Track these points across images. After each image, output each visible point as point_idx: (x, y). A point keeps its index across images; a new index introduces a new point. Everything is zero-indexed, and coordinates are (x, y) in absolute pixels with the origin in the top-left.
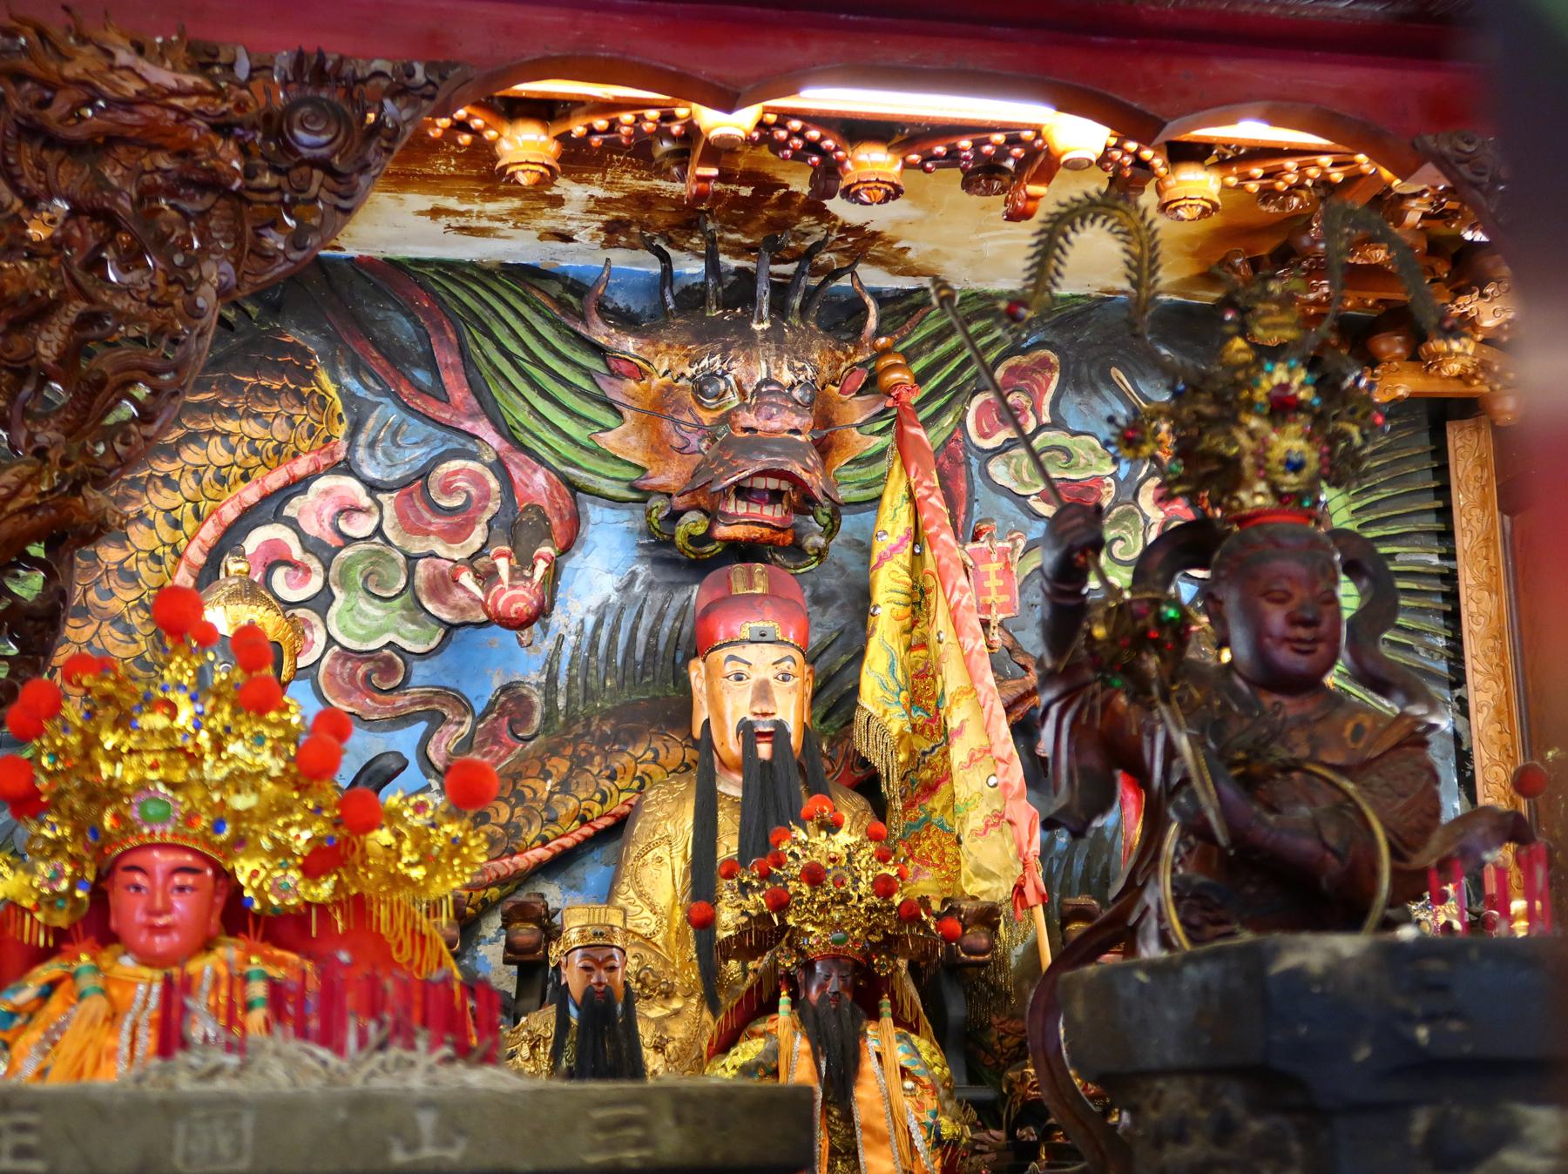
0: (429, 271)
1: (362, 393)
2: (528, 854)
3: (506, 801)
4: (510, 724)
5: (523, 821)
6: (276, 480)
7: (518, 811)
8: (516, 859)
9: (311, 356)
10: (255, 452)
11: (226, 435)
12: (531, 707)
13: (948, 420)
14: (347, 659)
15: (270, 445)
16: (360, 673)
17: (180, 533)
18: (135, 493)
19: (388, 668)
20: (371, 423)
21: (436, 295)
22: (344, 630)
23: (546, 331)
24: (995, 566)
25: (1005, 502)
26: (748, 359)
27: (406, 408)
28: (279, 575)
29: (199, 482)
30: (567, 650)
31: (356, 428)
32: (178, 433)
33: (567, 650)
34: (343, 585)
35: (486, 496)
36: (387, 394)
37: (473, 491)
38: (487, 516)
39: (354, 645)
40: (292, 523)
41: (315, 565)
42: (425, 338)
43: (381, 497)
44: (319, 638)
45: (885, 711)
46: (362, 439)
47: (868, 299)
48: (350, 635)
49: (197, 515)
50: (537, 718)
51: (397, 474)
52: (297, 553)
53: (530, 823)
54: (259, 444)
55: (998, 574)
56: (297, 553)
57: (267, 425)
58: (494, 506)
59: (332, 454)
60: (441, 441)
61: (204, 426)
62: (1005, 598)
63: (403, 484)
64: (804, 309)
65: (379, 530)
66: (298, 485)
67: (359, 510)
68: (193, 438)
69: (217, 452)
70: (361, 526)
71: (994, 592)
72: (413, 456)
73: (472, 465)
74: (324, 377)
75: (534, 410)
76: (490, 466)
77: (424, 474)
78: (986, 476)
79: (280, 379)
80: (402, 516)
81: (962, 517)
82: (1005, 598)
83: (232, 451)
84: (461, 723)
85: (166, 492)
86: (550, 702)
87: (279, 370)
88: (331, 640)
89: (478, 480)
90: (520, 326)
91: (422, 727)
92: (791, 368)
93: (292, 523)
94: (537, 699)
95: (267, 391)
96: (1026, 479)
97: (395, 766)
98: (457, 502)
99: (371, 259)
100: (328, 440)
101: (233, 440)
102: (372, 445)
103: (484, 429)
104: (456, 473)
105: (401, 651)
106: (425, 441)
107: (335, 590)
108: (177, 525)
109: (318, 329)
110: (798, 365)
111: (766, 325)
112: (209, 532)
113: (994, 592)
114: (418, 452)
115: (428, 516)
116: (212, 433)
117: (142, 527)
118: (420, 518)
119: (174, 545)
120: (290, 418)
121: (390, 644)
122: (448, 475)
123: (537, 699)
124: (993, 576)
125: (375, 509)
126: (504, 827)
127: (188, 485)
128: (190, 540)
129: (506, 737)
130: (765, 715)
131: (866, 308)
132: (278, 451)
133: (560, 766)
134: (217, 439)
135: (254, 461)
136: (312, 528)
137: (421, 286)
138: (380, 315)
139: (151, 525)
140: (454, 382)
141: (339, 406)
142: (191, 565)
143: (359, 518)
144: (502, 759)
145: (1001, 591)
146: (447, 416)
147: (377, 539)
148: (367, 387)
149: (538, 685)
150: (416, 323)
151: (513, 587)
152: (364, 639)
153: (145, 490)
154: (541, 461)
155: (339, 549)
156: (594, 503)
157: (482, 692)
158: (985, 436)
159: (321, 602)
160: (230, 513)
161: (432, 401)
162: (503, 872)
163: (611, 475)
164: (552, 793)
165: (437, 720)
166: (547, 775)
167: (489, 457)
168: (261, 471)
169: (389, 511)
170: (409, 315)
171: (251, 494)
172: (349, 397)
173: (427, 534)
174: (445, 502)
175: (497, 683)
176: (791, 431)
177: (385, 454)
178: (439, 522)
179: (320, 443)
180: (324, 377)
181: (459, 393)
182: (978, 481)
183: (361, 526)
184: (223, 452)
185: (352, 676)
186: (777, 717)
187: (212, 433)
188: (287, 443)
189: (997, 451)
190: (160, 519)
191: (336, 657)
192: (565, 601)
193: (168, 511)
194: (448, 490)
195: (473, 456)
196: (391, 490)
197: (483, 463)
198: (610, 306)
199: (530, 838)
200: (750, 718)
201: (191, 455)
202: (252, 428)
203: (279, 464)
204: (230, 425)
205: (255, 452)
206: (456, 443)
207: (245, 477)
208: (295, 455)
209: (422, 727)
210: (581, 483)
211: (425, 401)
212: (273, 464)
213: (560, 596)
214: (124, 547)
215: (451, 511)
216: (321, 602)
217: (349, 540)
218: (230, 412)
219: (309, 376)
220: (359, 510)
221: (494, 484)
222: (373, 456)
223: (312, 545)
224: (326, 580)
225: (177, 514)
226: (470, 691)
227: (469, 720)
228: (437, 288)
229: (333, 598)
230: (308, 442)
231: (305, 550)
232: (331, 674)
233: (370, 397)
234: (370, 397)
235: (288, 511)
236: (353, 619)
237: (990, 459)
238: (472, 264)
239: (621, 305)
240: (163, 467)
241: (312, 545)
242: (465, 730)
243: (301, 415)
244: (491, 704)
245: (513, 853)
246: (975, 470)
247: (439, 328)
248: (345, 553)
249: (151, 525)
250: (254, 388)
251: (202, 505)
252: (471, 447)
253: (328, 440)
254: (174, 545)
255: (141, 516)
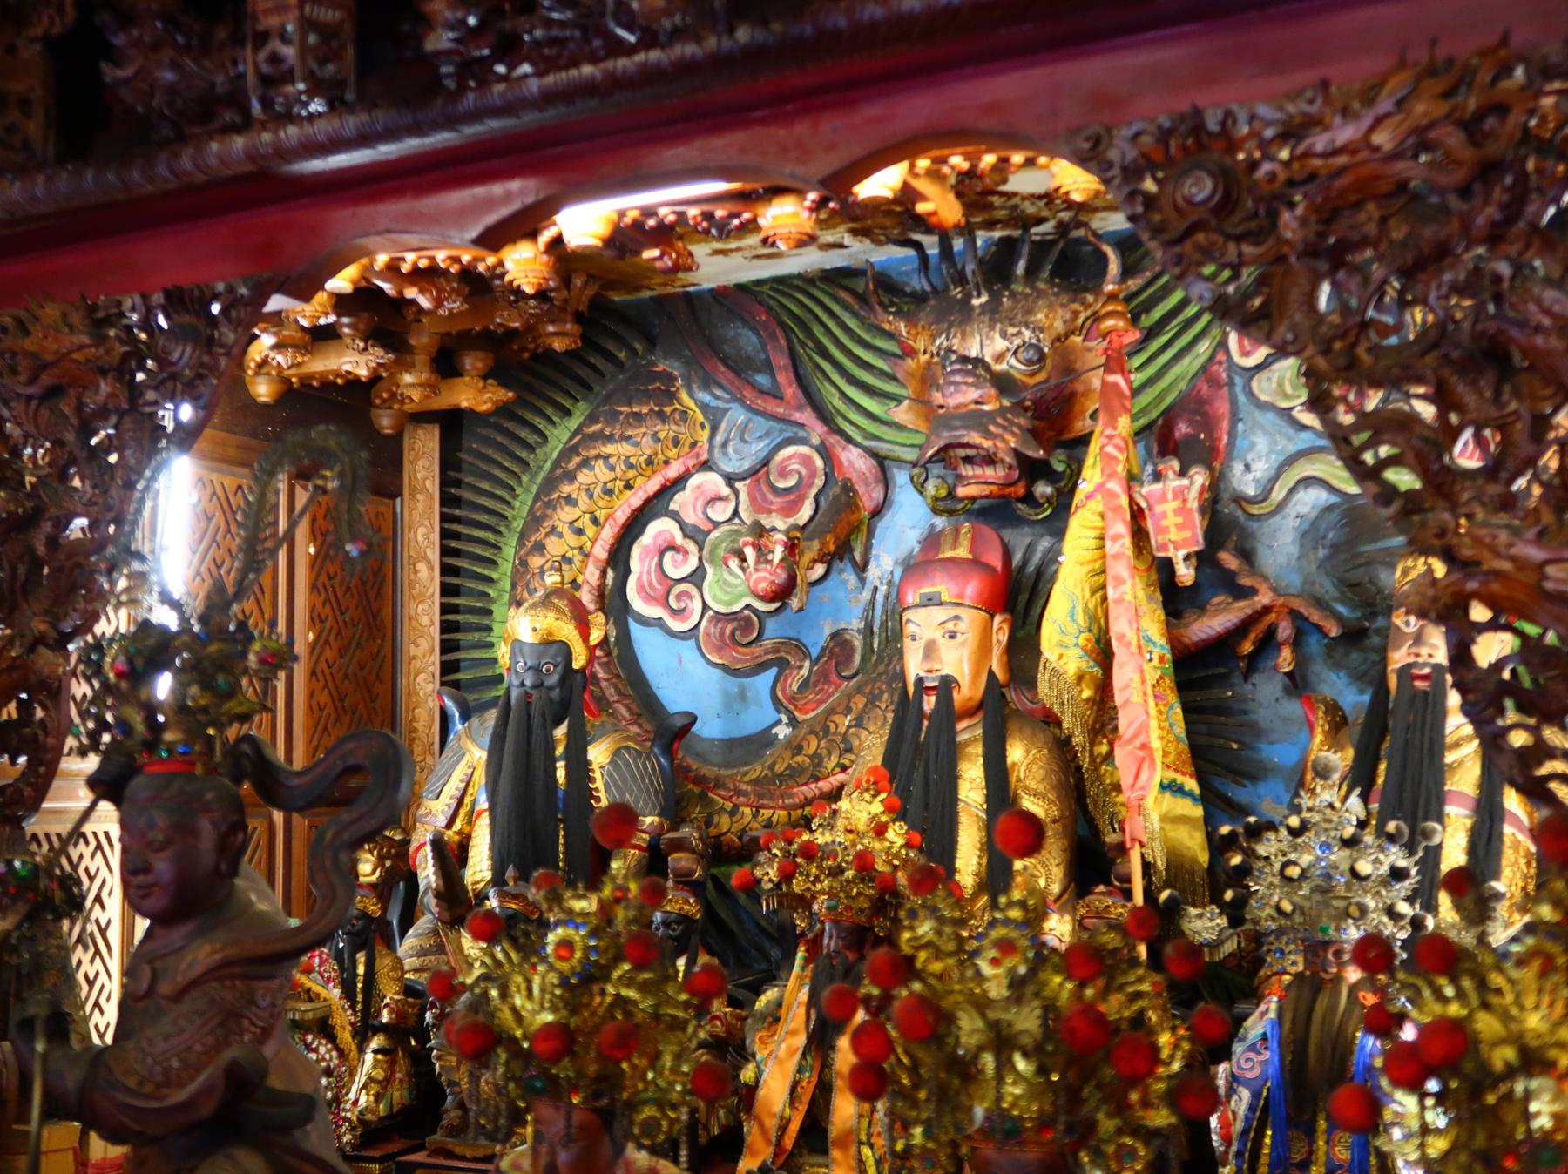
0: (765, 289)
1: (714, 403)
2: (831, 779)
3: (816, 734)
4: (837, 665)
5: (825, 752)
6: (653, 485)
7: (823, 743)
8: (821, 784)
9: (675, 379)
10: (631, 466)
11: (606, 458)
12: (852, 650)
13: (1204, 347)
14: (719, 621)
15: (642, 459)
16: (728, 631)
17: (584, 538)
18: (549, 512)
19: (746, 625)
20: (723, 426)
21: (770, 308)
22: (714, 598)
23: (852, 323)
24: (1171, 505)
25: (1270, 416)
26: (964, 336)
27: (750, 409)
28: (668, 556)
29: (591, 496)
30: (880, 598)
31: (714, 431)
32: (577, 460)
33: (880, 598)
34: (712, 562)
35: (813, 475)
36: (734, 399)
37: (804, 471)
38: (814, 491)
39: (722, 609)
40: (676, 516)
41: (692, 547)
42: (764, 349)
43: (739, 485)
44: (697, 606)
45: (1061, 657)
46: (719, 439)
47: (1108, 250)
48: (719, 602)
49: (595, 521)
50: (857, 658)
51: (746, 465)
52: (679, 539)
53: (830, 754)
54: (632, 460)
55: (1177, 512)
56: (679, 539)
57: (636, 444)
58: (819, 482)
59: (698, 455)
60: (780, 432)
61: (593, 452)
62: (1187, 534)
63: (753, 473)
64: (1031, 272)
65: (736, 513)
66: (678, 483)
67: (720, 498)
68: (585, 463)
69: (601, 472)
70: (721, 512)
71: (1173, 529)
72: (758, 448)
73: (803, 449)
74: (684, 396)
75: (843, 395)
76: (818, 450)
77: (766, 462)
78: (1250, 394)
79: (647, 404)
80: (752, 499)
81: (1225, 439)
82: (1187, 534)
83: (612, 468)
84: (801, 667)
85: (567, 509)
86: (868, 646)
87: (647, 396)
88: (705, 607)
89: (806, 461)
90: (839, 322)
91: (773, 671)
92: (1004, 335)
93: (676, 516)
94: (858, 643)
95: (638, 416)
96: (1289, 390)
97: (687, 721)
98: (791, 482)
99: (725, 288)
100: (693, 445)
101: (612, 461)
102: (724, 445)
103: (806, 416)
104: (790, 458)
105: (755, 611)
106: (767, 434)
107: (707, 566)
108: (580, 532)
109: (678, 355)
110: (1011, 330)
111: (984, 299)
112: (608, 534)
113: (1173, 529)
114: (761, 445)
115: (770, 497)
116: (598, 456)
117: (553, 538)
118: (765, 499)
119: (581, 548)
120: (655, 435)
121: (748, 606)
122: (784, 460)
123: (858, 643)
124: (1171, 515)
125: (732, 497)
126: (811, 757)
127: (583, 500)
128: (593, 543)
129: (834, 677)
130: (929, 671)
131: (1104, 259)
132: (649, 462)
133: (859, 702)
134: (601, 462)
135: (631, 474)
136: (691, 517)
137: (760, 303)
138: (731, 333)
139: (561, 535)
140: (785, 380)
141: (700, 417)
142: (597, 560)
143: (719, 505)
144: (829, 696)
145: (1180, 527)
146: (781, 410)
147: (737, 521)
148: (717, 398)
149: (859, 631)
150: (758, 335)
151: (757, 570)
152: (729, 604)
153: (555, 509)
154: (849, 440)
155: (710, 531)
156: (899, 468)
157: (817, 639)
158: (1246, 354)
159: (697, 577)
160: (622, 515)
161: (771, 399)
162: (810, 795)
163: (908, 442)
164: (849, 727)
165: (782, 664)
166: (848, 710)
167: (816, 441)
168: (640, 480)
169: (743, 497)
170: (754, 329)
171: (636, 499)
172: (704, 407)
173: (769, 512)
174: (781, 484)
175: (827, 631)
176: (977, 403)
177: (736, 451)
178: (778, 500)
179: (687, 449)
180: (684, 396)
181: (791, 390)
182: (1242, 399)
183: (721, 512)
184: (605, 470)
185: (722, 633)
186: (944, 673)
187: (598, 456)
188: (656, 454)
189: (1259, 368)
190: (565, 530)
191: (712, 618)
192: (878, 557)
193: (571, 523)
194: (783, 474)
195: (804, 441)
196: (744, 479)
197: (812, 446)
198: (908, 290)
199: (830, 766)
200: (922, 674)
201: (584, 477)
202: (624, 449)
203: (654, 472)
204: (609, 449)
205: (631, 466)
206: (790, 432)
207: (628, 487)
208: (667, 463)
209: (773, 671)
210: (883, 453)
211: (765, 401)
212: (649, 472)
213: (874, 552)
214: (543, 555)
215: (787, 490)
216: (697, 577)
217: (716, 524)
218: (610, 439)
219: (671, 397)
220: (720, 498)
221: (819, 463)
222: (725, 454)
223: (690, 532)
224: (700, 559)
225: (579, 524)
226: (808, 640)
227: (807, 664)
228: (772, 302)
229: (705, 572)
230: (675, 451)
231: (685, 536)
232: (707, 634)
233: (720, 404)
234: (720, 404)
235: (673, 506)
236: (721, 588)
237: (1252, 378)
238: (799, 276)
239: (918, 287)
240: (567, 489)
241: (690, 532)
242: (805, 672)
243: (665, 431)
244: (823, 649)
245: (817, 780)
246: (1238, 389)
247: (773, 336)
248: (713, 535)
249: (561, 535)
250: (628, 415)
251: (598, 514)
252: (801, 434)
253: (693, 445)
254: (581, 548)
255: (554, 528)
